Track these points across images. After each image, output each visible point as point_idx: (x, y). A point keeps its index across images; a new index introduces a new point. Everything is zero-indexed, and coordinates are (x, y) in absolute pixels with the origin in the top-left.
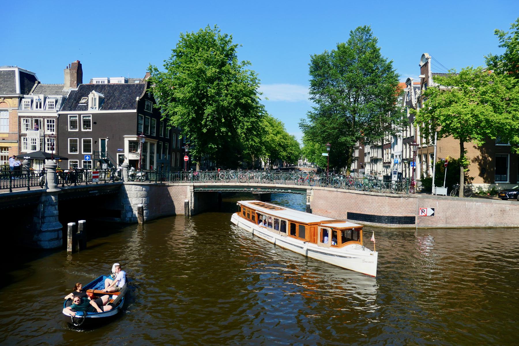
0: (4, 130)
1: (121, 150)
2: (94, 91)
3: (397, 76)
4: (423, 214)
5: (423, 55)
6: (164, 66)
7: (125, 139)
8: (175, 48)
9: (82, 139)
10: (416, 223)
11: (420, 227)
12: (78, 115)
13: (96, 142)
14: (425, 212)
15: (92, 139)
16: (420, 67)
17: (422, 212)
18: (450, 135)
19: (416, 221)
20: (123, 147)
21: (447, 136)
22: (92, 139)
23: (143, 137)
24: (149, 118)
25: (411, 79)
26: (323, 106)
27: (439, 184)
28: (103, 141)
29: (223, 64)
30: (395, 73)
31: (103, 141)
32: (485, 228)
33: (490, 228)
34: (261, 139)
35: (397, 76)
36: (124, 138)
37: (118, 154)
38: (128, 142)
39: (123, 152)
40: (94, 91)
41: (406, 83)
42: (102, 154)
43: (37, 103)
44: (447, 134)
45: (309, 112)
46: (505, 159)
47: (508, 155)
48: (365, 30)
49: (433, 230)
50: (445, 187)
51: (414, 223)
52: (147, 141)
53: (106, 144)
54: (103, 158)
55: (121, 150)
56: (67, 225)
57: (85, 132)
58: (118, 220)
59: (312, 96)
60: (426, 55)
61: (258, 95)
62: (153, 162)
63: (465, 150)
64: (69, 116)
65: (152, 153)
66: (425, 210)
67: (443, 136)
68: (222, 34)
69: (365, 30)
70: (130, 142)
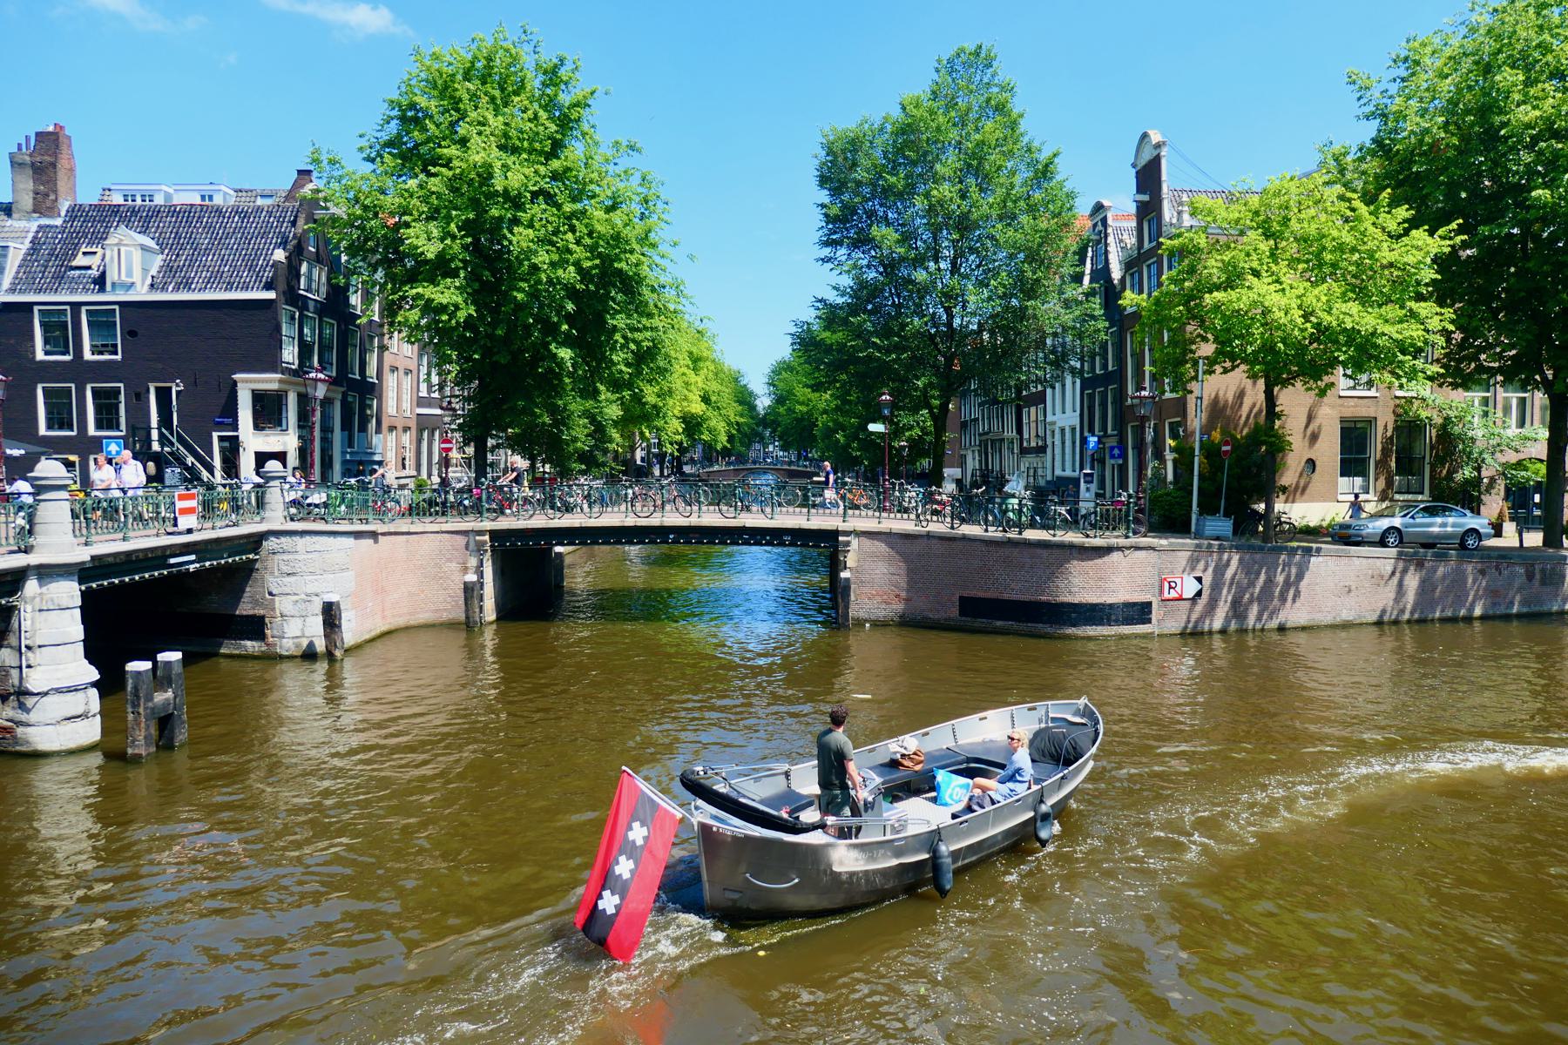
0: (1064, 470)
3: (1071, 196)
4: (1173, 594)
5: (1145, 136)
6: (361, 149)
8: (395, 96)
10: (1154, 620)
11: (1166, 631)
13: (139, 397)
14: (1178, 589)
16: (1134, 171)
17: (1170, 587)
18: (1238, 366)
19: (1155, 615)
21: (1226, 371)
23: (320, 380)
25: (1106, 203)
26: (862, 284)
27: (1208, 508)
29: (557, 147)
30: (1068, 186)
32: (1333, 627)
33: (1346, 626)
35: (1071, 196)
41: (1091, 215)
42: (161, 435)
44: (1228, 364)
45: (820, 301)
48: (979, 59)
49: (368, 650)
50: (1227, 515)
51: (1149, 621)
52: (331, 395)
54: (167, 449)
56: (124, 672)
57: (49, 362)
58: (251, 646)
59: (827, 251)
60: (1152, 136)
61: (662, 248)
62: (331, 458)
63: (1277, 409)
64: (36, 308)
65: (327, 430)
66: (1178, 581)
67: (1214, 372)
68: (548, 57)
69: (979, 59)
70: (259, 398)
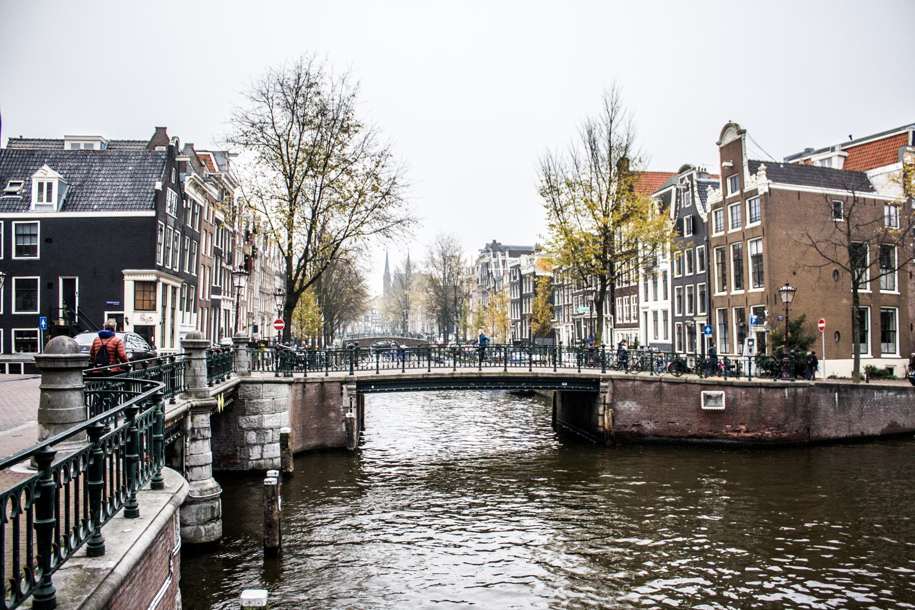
1: (115, 303)
2: (46, 167)
7: (126, 278)
9: (14, 279)
12: (39, 222)
13: (49, 287)
15: (39, 278)
20: (120, 296)
22: (39, 278)
24: (171, 230)
28: (69, 285)
31: (69, 285)
34: (530, 356)
36: (123, 275)
37: (106, 313)
38: (132, 284)
39: (121, 307)
40: (46, 167)
43: (49, 199)
46: (893, 314)
47: (895, 310)
53: (77, 290)
55: (115, 303)
